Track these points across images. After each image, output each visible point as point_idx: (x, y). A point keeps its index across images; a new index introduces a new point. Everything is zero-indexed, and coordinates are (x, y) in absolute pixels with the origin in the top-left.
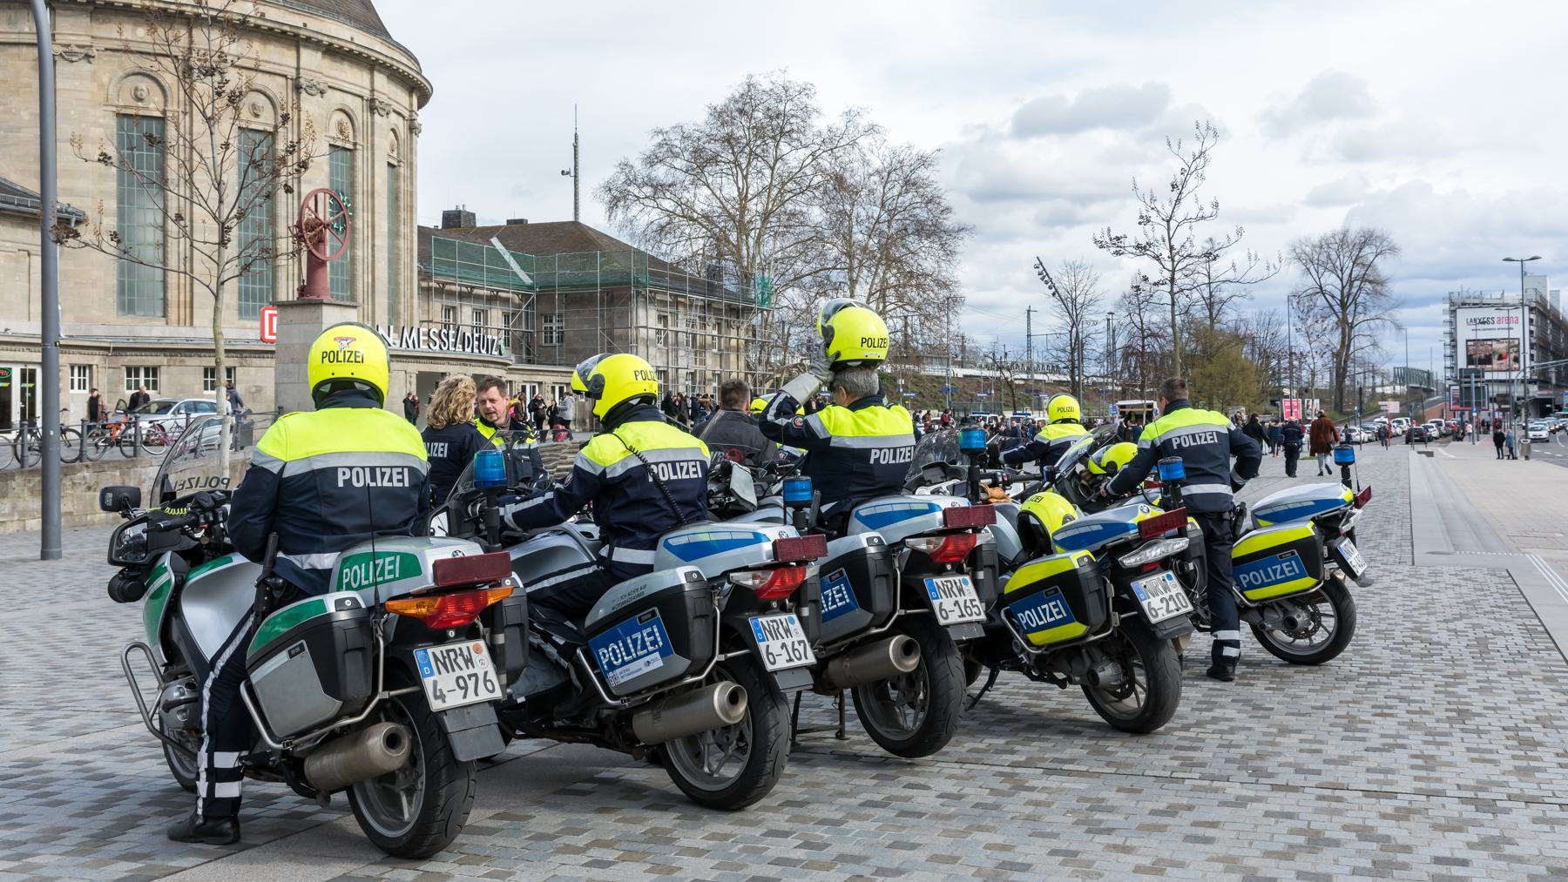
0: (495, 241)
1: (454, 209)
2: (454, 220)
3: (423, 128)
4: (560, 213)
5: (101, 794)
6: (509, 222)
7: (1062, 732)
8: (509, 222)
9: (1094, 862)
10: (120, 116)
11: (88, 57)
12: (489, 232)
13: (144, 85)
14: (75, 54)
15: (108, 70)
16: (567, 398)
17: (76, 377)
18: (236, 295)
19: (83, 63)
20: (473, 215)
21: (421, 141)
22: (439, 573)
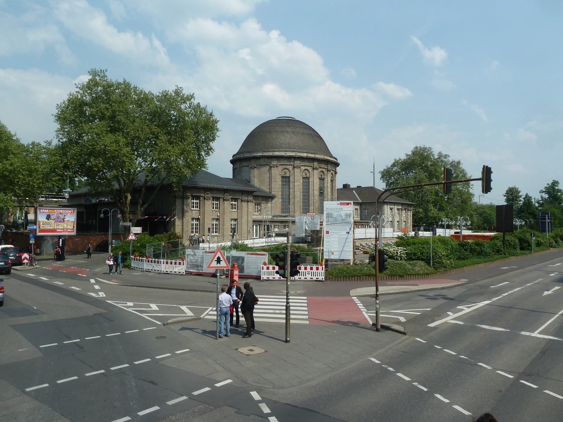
0: (354, 191)
1: (345, 184)
2: (346, 186)
3: (504, 192)
4: (370, 184)
5: (249, 181)
6: (357, 186)
7: (265, 157)
8: (357, 186)
9: (235, 412)
10: (320, 179)
11: (277, 167)
12: (353, 189)
13: (306, 171)
14: (274, 166)
15: (280, 168)
16: (329, 220)
17: (256, 207)
18: (281, 181)
19: (276, 168)
20: (350, 185)
21: (337, 175)
22: (240, 257)
